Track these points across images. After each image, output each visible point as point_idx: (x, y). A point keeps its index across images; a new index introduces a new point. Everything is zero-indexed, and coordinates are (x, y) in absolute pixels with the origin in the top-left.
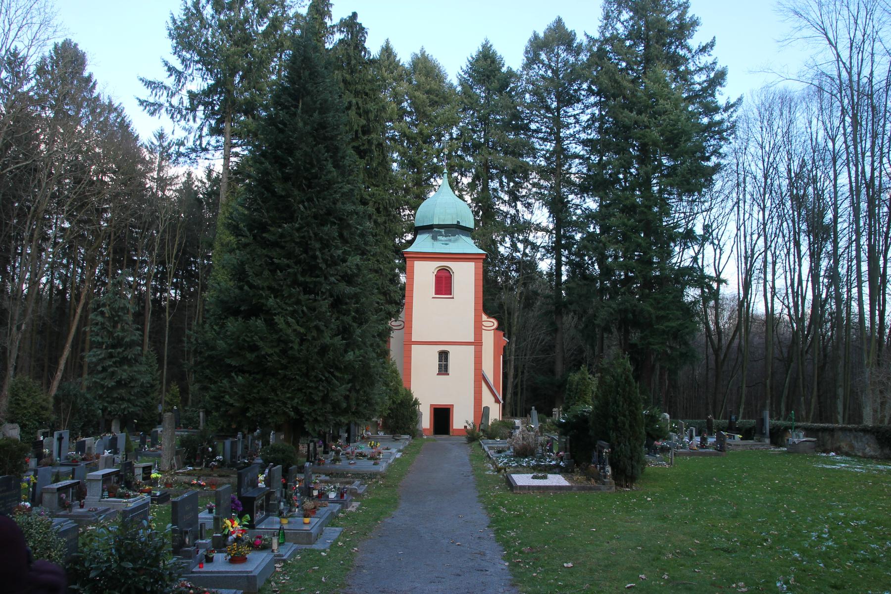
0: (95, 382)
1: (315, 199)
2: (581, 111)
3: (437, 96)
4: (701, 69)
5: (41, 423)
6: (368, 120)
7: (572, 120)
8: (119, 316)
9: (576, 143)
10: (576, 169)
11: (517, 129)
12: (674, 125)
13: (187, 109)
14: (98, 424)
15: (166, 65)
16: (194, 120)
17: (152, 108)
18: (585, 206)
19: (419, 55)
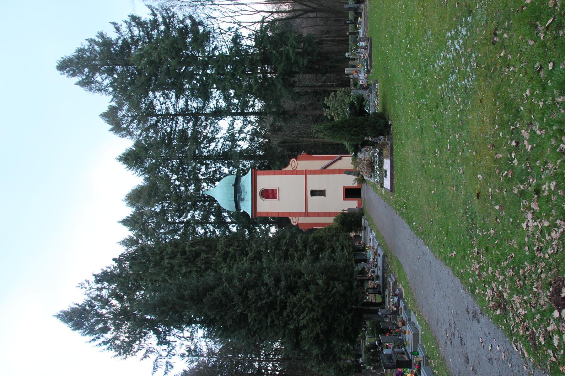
1: (234, 303)
2: (158, 101)
4: (130, 30)
6: (178, 252)
7: (164, 106)
9: (178, 104)
10: (194, 104)
11: (170, 140)
13: (169, 347)
15: (142, 359)
16: (175, 342)
17: (169, 367)
18: (217, 97)
19: (127, 202)
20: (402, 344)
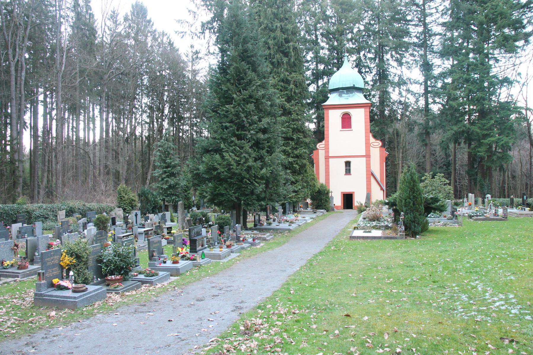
0: (158, 187)
3: (347, 5)
5: (133, 208)
8: (168, 151)
10: (436, 42)
11: (398, 21)
12: (496, 9)
14: (161, 207)
17: (182, 35)
20: (211, 245)
